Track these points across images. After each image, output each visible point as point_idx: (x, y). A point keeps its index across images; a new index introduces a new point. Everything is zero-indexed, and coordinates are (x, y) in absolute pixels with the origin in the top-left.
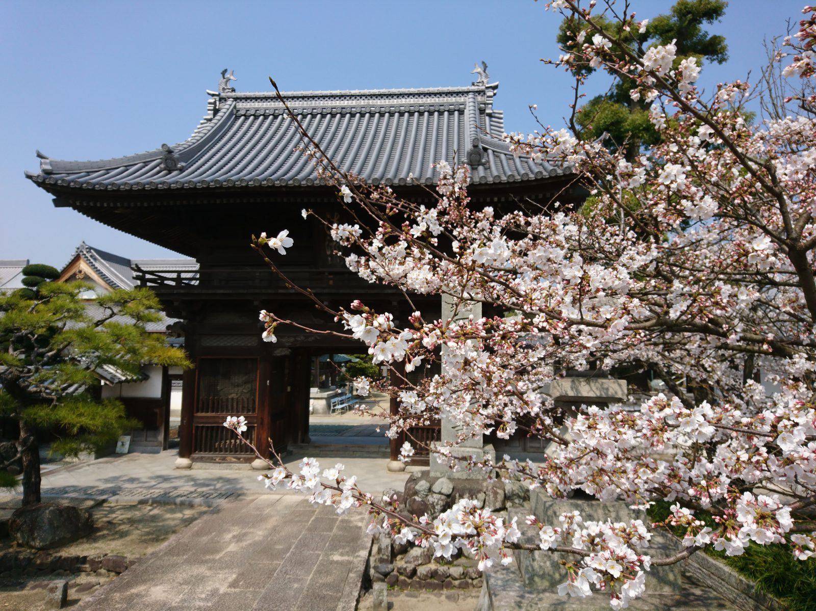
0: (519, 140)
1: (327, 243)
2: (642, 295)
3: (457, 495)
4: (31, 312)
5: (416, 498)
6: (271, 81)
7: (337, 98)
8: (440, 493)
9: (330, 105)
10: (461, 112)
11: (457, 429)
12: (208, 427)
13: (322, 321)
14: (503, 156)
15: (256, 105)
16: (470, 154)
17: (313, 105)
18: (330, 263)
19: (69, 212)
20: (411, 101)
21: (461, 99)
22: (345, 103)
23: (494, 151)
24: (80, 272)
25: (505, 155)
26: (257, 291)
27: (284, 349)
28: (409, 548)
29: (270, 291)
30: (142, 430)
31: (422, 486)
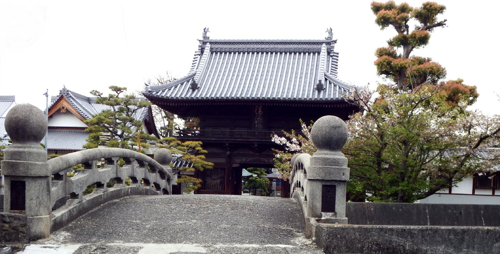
1: (256, 118)
7: (260, 44)
10: (319, 53)
15: (221, 46)
17: (248, 47)
18: (257, 127)
20: (295, 46)
21: (319, 46)
22: (263, 46)
24: (63, 108)
25: (344, 88)
26: (228, 139)
28: (347, 182)
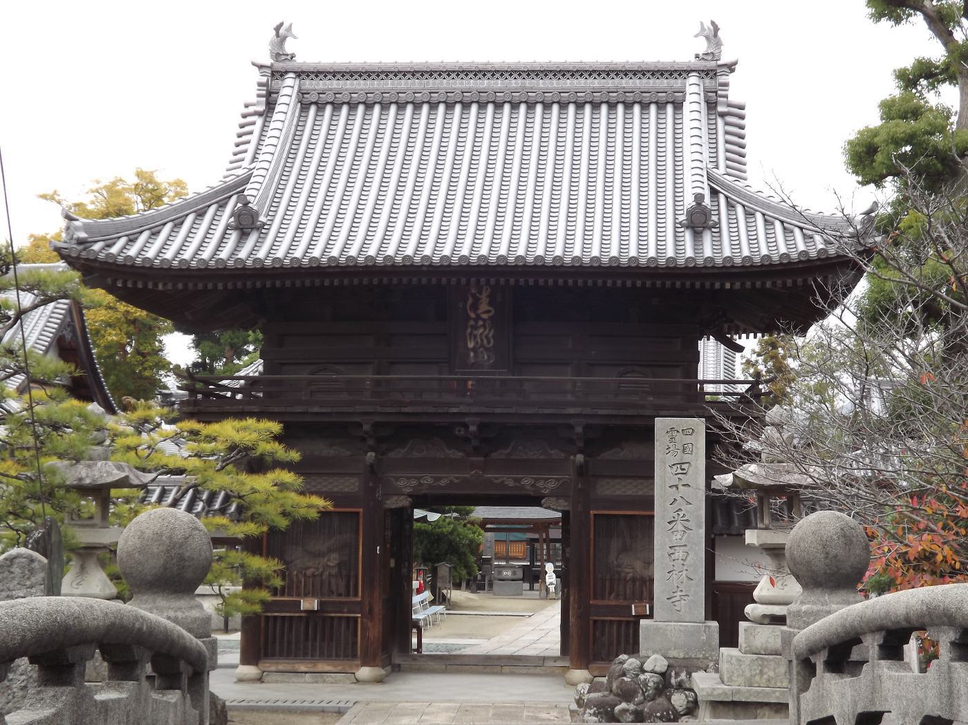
1: (469, 330)
3: (673, 674)
4: (687, 520)
8: (652, 671)
9: (362, 87)
10: (678, 106)
11: (673, 600)
12: (275, 617)
13: (460, 454)
14: (740, 209)
16: (691, 213)
20: (596, 83)
21: (677, 83)
23: (727, 197)
25: (744, 206)
27: (402, 498)
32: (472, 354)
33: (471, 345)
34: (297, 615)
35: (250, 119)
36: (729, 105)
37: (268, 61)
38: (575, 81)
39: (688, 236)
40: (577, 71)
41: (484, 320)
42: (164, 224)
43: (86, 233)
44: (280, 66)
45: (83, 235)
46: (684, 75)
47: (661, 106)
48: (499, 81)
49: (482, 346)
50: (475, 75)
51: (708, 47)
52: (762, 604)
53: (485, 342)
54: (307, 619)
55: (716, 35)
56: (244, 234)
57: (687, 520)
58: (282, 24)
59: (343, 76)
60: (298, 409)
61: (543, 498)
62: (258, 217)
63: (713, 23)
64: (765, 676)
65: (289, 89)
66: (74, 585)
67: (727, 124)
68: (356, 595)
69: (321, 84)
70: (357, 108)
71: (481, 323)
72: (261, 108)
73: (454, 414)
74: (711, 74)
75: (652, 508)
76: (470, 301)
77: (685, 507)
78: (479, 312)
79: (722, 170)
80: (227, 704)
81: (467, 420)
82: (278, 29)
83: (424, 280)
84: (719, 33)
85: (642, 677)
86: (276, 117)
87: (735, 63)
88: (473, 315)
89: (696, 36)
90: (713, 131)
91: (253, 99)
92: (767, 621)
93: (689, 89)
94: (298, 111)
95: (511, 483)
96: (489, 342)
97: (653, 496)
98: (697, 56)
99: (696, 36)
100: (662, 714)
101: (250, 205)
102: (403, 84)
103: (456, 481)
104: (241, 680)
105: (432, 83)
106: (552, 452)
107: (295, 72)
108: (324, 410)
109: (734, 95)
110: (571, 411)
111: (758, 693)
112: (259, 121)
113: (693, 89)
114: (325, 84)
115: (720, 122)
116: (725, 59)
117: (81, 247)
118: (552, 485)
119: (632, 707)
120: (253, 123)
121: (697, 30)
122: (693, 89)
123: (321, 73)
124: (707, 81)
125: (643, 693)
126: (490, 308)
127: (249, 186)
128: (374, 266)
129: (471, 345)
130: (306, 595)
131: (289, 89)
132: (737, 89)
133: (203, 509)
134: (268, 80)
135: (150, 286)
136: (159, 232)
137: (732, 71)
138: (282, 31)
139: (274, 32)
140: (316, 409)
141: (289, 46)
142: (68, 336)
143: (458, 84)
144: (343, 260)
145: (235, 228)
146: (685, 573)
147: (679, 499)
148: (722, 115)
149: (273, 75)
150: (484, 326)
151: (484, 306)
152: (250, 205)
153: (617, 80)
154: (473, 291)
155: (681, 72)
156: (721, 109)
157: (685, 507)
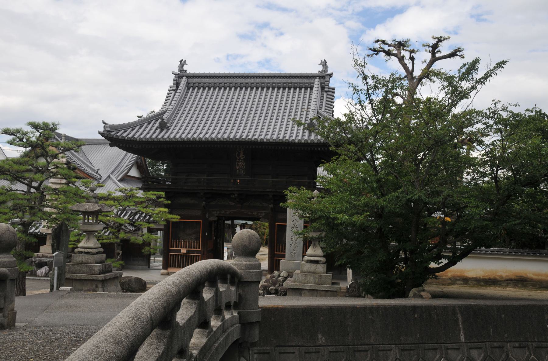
0: (369, 103)
1: (237, 163)
2: (431, 187)
4: (297, 227)
5: (274, 279)
6: (503, 62)
9: (208, 81)
10: (312, 89)
11: (292, 253)
12: (176, 255)
16: (309, 124)
17: (230, 81)
19: (115, 149)
22: (248, 81)
29: (208, 188)
30: (430, 298)
31: (276, 274)
32: (238, 171)
33: (237, 168)
34: (180, 254)
35: (171, 92)
36: (329, 88)
37: (177, 72)
38: (278, 80)
39: (307, 132)
40: (279, 77)
41: (242, 160)
42: (137, 126)
43: (110, 128)
44: (181, 74)
45: (109, 129)
46: (315, 78)
47: (306, 89)
48: (253, 80)
49: (241, 168)
50: (245, 78)
51: (323, 69)
52: (308, 256)
53: (242, 167)
54: (183, 255)
55: (326, 64)
56: (162, 130)
57: (297, 227)
58: (182, 60)
59: (213, 78)
60: (180, 187)
61: (260, 218)
62: (167, 124)
63: (325, 60)
64: (306, 280)
65: (184, 81)
66: (85, 243)
67: (328, 95)
68: (199, 248)
69: (194, 80)
70: (200, 88)
71: (241, 160)
72: (174, 88)
73: (214, 190)
74: (324, 78)
75: (286, 223)
76: (237, 153)
77: (296, 223)
78: (240, 157)
79: (323, 110)
80: (147, 282)
81: (234, 192)
82: (181, 62)
83: (187, 146)
84: (327, 64)
85: (279, 278)
86: (178, 91)
87: (332, 74)
88: (238, 158)
89: (319, 65)
90: (322, 97)
91: (172, 85)
92: (309, 262)
93: (316, 83)
94: (186, 89)
95: (250, 214)
96: (243, 167)
97: (286, 219)
98: (319, 71)
99: (319, 65)
100: (284, 291)
101: (164, 120)
102: (221, 81)
103: (232, 212)
104: (162, 274)
105: (230, 80)
106: (264, 204)
107: (186, 76)
108: (188, 188)
109: (331, 85)
110: (268, 190)
111: (303, 285)
112: (173, 92)
113: (317, 83)
114: (196, 81)
115: (325, 94)
116: (329, 72)
117: (108, 133)
118: (263, 214)
119: (274, 288)
120: (172, 93)
121: (320, 62)
122: (317, 83)
123: (195, 77)
124: (322, 80)
125: (279, 284)
126: (243, 156)
127: (166, 114)
128: (257, 142)
129: (237, 168)
130: (184, 248)
131: (184, 81)
132: (332, 83)
133: (142, 219)
134: (177, 79)
135: (131, 146)
136: (135, 129)
137: (331, 77)
138: (182, 62)
139: (180, 63)
140: (186, 188)
141: (185, 67)
142: (139, 162)
143: (239, 81)
144: (240, 139)
145: (159, 128)
146: (296, 245)
147: (295, 220)
148: (326, 92)
149: (179, 77)
150: (242, 161)
151: (241, 155)
152: (164, 120)
153: (292, 80)
154: (238, 150)
155: (312, 77)
156: (326, 90)
157: (296, 223)
